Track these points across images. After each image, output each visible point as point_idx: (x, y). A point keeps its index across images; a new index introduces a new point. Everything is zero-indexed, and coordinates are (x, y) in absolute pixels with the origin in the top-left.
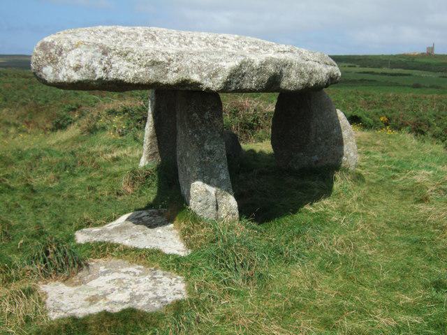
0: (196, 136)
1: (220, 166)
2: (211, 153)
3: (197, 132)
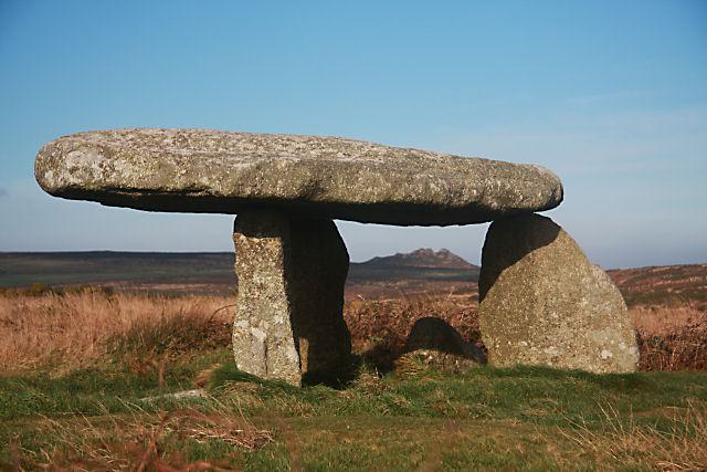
1: (275, 306)
2: (262, 287)
3: (246, 260)
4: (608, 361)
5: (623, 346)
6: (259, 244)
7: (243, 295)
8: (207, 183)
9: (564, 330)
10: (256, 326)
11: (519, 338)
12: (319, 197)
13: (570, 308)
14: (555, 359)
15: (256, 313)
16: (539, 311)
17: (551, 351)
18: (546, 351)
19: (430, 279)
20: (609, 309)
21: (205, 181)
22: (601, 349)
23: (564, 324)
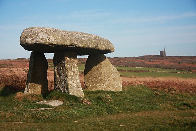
0: (68, 66)
2: (74, 72)
3: (69, 65)
4: (117, 89)
5: (120, 85)
6: (73, 60)
7: (70, 74)
8: (77, 44)
9: (107, 82)
10: (73, 83)
11: (97, 84)
12: (97, 48)
13: (109, 76)
14: (105, 89)
15: (74, 80)
16: (103, 77)
17: (104, 87)
18: (103, 86)
19: (157, 67)
20: (117, 76)
21: (76, 43)
22: (115, 86)
23: (108, 80)
